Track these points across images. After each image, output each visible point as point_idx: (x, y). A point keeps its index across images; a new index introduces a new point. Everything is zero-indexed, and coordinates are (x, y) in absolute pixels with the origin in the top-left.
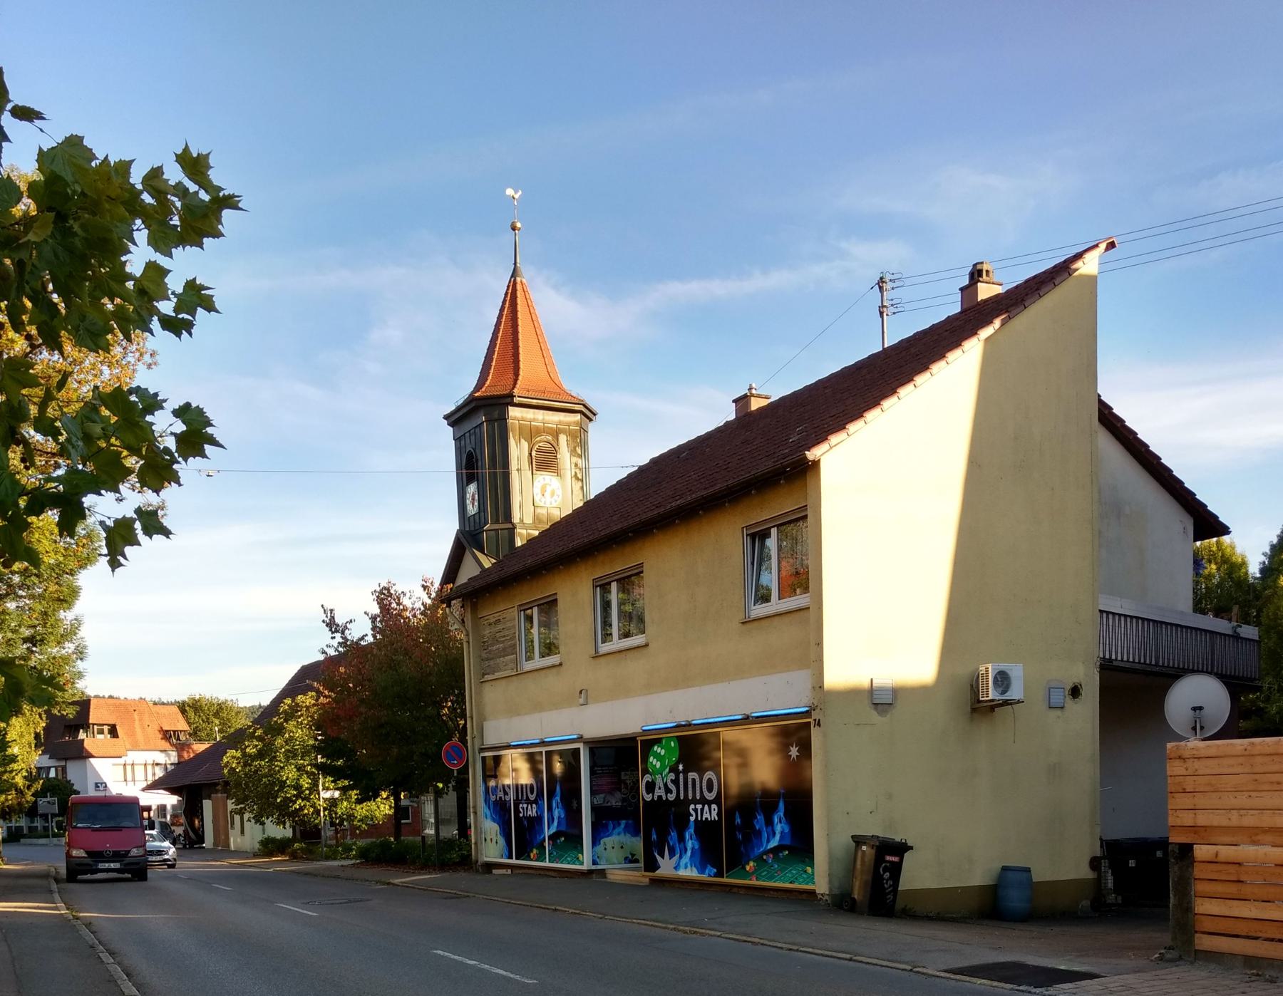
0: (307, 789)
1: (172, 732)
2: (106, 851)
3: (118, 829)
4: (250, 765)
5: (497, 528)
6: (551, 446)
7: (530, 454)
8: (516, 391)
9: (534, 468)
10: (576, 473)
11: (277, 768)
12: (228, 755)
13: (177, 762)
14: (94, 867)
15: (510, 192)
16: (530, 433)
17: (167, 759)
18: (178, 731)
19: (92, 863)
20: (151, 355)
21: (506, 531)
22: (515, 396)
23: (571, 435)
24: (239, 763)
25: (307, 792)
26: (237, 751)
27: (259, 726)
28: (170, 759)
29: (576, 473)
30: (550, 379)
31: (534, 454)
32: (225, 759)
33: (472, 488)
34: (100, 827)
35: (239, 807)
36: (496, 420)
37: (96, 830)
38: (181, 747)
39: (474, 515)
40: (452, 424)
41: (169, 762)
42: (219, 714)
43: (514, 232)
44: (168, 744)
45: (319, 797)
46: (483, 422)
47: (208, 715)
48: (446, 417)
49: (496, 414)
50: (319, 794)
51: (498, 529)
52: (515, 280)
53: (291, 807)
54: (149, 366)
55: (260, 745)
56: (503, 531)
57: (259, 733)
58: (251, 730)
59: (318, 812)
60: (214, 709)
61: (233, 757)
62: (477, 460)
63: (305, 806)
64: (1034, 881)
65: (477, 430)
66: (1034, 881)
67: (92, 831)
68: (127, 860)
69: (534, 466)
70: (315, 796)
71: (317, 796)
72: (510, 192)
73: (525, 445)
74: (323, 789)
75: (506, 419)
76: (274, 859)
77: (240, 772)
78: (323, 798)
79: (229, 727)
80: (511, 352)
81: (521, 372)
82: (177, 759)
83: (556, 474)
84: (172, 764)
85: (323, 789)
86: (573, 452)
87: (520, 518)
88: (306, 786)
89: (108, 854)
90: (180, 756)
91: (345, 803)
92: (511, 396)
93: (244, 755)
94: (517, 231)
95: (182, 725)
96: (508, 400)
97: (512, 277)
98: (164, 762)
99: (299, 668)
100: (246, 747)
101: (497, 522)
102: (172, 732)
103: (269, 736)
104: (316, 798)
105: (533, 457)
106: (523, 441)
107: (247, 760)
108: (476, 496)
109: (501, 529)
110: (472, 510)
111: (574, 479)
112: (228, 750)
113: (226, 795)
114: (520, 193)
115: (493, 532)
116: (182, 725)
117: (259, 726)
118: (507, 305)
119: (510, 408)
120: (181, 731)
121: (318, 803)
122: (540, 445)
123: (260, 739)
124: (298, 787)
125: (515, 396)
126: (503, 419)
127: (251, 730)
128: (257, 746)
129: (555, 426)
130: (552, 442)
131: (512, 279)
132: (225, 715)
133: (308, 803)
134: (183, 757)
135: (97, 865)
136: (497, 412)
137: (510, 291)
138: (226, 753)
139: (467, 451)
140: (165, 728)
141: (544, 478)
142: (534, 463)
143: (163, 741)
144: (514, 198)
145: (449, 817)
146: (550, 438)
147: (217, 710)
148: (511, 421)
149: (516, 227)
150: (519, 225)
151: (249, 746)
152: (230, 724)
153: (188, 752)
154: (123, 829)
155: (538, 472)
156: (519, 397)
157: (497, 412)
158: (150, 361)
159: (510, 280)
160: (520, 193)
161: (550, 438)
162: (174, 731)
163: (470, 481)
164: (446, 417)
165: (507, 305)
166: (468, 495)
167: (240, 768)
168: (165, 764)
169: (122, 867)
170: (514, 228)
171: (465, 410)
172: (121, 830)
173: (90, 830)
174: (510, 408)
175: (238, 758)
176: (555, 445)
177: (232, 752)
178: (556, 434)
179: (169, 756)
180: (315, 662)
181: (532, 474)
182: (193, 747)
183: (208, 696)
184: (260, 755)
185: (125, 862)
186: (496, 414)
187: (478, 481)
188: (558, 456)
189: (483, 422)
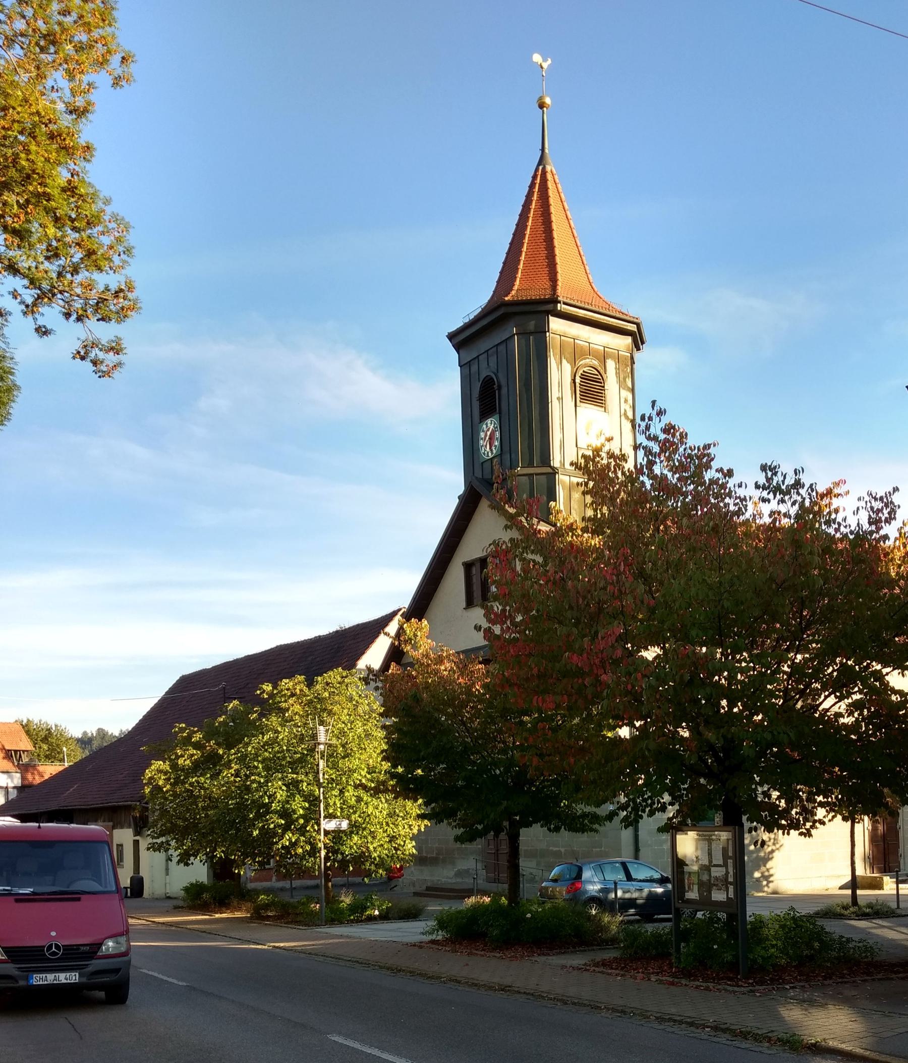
0: (302, 816)
1: (13, 752)
2: (50, 947)
3: (74, 896)
4: (183, 783)
5: (532, 472)
6: (597, 373)
7: (574, 381)
8: (560, 291)
9: (578, 399)
10: (625, 411)
11: (255, 785)
12: (153, 767)
13: (20, 785)
14: (22, 983)
15: (537, 58)
16: (575, 353)
17: (9, 781)
18: (20, 751)
19: (16, 973)
20: (123, 58)
21: (544, 477)
22: (560, 302)
23: (618, 359)
24: (169, 779)
25: (301, 821)
26: (164, 762)
27: (196, 729)
28: (12, 781)
29: (625, 411)
30: (593, 291)
31: (578, 380)
32: (148, 774)
33: (490, 425)
34: (34, 893)
35: (159, 841)
36: (531, 333)
37: (21, 899)
38: (25, 769)
39: (492, 459)
40: (458, 347)
41: (11, 785)
42: (48, 740)
43: (541, 111)
44: (11, 764)
45: (319, 829)
46: (514, 335)
47: (36, 740)
48: (451, 337)
49: (532, 325)
50: (319, 825)
51: (532, 475)
52: (544, 168)
53: (277, 843)
54: (117, 82)
55: (197, 754)
56: (538, 477)
57: (197, 737)
58: (185, 734)
59: (314, 851)
60: (43, 734)
61: (160, 771)
62: (500, 387)
63: (297, 841)
64: (713, 899)
65: (502, 348)
66: (713, 899)
67: (17, 901)
68: (95, 965)
69: (578, 395)
70: (313, 826)
71: (316, 828)
72: (537, 58)
73: (567, 368)
74: (325, 817)
75: (546, 332)
76: (217, 916)
77: (167, 791)
78: (325, 830)
79: (58, 753)
80: (544, 253)
81: (559, 277)
82: (20, 781)
83: (603, 409)
84: (14, 788)
85: (325, 817)
86: (621, 384)
87: (561, 462)
88: (301, 812)
89: (54, 954)
90: (23, 778)
91: (356, 838)
92: (556, 301)
93: (174, 766)
94: (545, 109)
95: (25, 744)
96: (550, 307)
97: (539, 164)
98: (5, 785)
99: (178, 678)
100: (178, 757)
101: (531, 465)
102: (13, 752)
103: (212, 742)
104: (315, 830)
105: (578, 385)
106: (564, 361)
107: (178, 775)
108: (498, 434)
109: (537, 474)
110: (487, 450)
111: (623, 418)
112: (153, 762)
113: (111, 824)
114: (549, 61)
115: (526, 478)
116: (25, 744)
117: (196, 729)
118: (535, 197)
119: (551, 318)
120: (24, 751)
121: (318, 837)
122: (585, 369)
123: (198, 746)
124: (286, 814)
125: (560, 302)
126: (542, 331)
127: (185, 734)
128: (192, 755)
129: (602, 348)
130: (599, 369)
131: (541, 168)
132: (54, 741)
133: (302, 838)
134: (27, 779)
135: (27, 979)
136: (533, 323)
137: (538, 181)
138: (151, 765)
139: (482, 377)
140: (7, 748)
141: (588, 411)
142: (578, 392)
143: (5, 761)
144: (542, 67)
145: (434, 855)
146: (595, 363)
147: (46, 736)
148: (551, 335)
149: (544, 103)
150: (548, 101)
151: (182, 756)
152: (59, 750)
153: (33, 774)
154: (83, 897)
155: (582, 404)
156: (565, 303)
157: (533, 323)
158: (119, 71)
159: (537, 170)
160: (549, 61)
161: (595, 363)
162: (16, 751)
163: (485, 414)
164: (451, 337)
165: (535, 197)
166: (482, 435)
167: (168, 787)
168: (7, 788)
169: (84, 980)
170: (542, 106)
171: (484, 322)
172: (79, 899)
173: (12, 898)
174: (551, 318)
175: (166, 773)
176: (602, 372)
177: (158, 764)
178: (603, 358)
179: (12, 778)
180: (225, 663)
181: (576, 406)
182: (38, 768)
183: (36, 721)
184: (197, 767)
185: (90, 969)
186: (532, 325)
187: (500, 413)
188: (606, 387)
189: (514, 335)
